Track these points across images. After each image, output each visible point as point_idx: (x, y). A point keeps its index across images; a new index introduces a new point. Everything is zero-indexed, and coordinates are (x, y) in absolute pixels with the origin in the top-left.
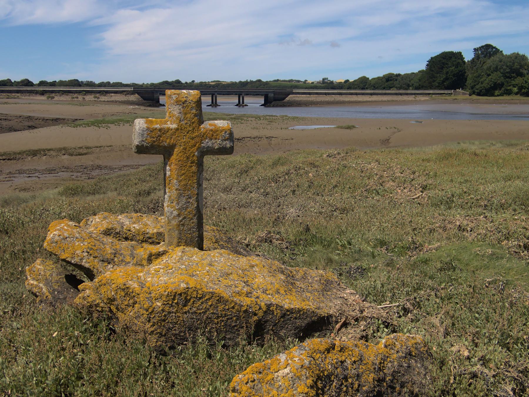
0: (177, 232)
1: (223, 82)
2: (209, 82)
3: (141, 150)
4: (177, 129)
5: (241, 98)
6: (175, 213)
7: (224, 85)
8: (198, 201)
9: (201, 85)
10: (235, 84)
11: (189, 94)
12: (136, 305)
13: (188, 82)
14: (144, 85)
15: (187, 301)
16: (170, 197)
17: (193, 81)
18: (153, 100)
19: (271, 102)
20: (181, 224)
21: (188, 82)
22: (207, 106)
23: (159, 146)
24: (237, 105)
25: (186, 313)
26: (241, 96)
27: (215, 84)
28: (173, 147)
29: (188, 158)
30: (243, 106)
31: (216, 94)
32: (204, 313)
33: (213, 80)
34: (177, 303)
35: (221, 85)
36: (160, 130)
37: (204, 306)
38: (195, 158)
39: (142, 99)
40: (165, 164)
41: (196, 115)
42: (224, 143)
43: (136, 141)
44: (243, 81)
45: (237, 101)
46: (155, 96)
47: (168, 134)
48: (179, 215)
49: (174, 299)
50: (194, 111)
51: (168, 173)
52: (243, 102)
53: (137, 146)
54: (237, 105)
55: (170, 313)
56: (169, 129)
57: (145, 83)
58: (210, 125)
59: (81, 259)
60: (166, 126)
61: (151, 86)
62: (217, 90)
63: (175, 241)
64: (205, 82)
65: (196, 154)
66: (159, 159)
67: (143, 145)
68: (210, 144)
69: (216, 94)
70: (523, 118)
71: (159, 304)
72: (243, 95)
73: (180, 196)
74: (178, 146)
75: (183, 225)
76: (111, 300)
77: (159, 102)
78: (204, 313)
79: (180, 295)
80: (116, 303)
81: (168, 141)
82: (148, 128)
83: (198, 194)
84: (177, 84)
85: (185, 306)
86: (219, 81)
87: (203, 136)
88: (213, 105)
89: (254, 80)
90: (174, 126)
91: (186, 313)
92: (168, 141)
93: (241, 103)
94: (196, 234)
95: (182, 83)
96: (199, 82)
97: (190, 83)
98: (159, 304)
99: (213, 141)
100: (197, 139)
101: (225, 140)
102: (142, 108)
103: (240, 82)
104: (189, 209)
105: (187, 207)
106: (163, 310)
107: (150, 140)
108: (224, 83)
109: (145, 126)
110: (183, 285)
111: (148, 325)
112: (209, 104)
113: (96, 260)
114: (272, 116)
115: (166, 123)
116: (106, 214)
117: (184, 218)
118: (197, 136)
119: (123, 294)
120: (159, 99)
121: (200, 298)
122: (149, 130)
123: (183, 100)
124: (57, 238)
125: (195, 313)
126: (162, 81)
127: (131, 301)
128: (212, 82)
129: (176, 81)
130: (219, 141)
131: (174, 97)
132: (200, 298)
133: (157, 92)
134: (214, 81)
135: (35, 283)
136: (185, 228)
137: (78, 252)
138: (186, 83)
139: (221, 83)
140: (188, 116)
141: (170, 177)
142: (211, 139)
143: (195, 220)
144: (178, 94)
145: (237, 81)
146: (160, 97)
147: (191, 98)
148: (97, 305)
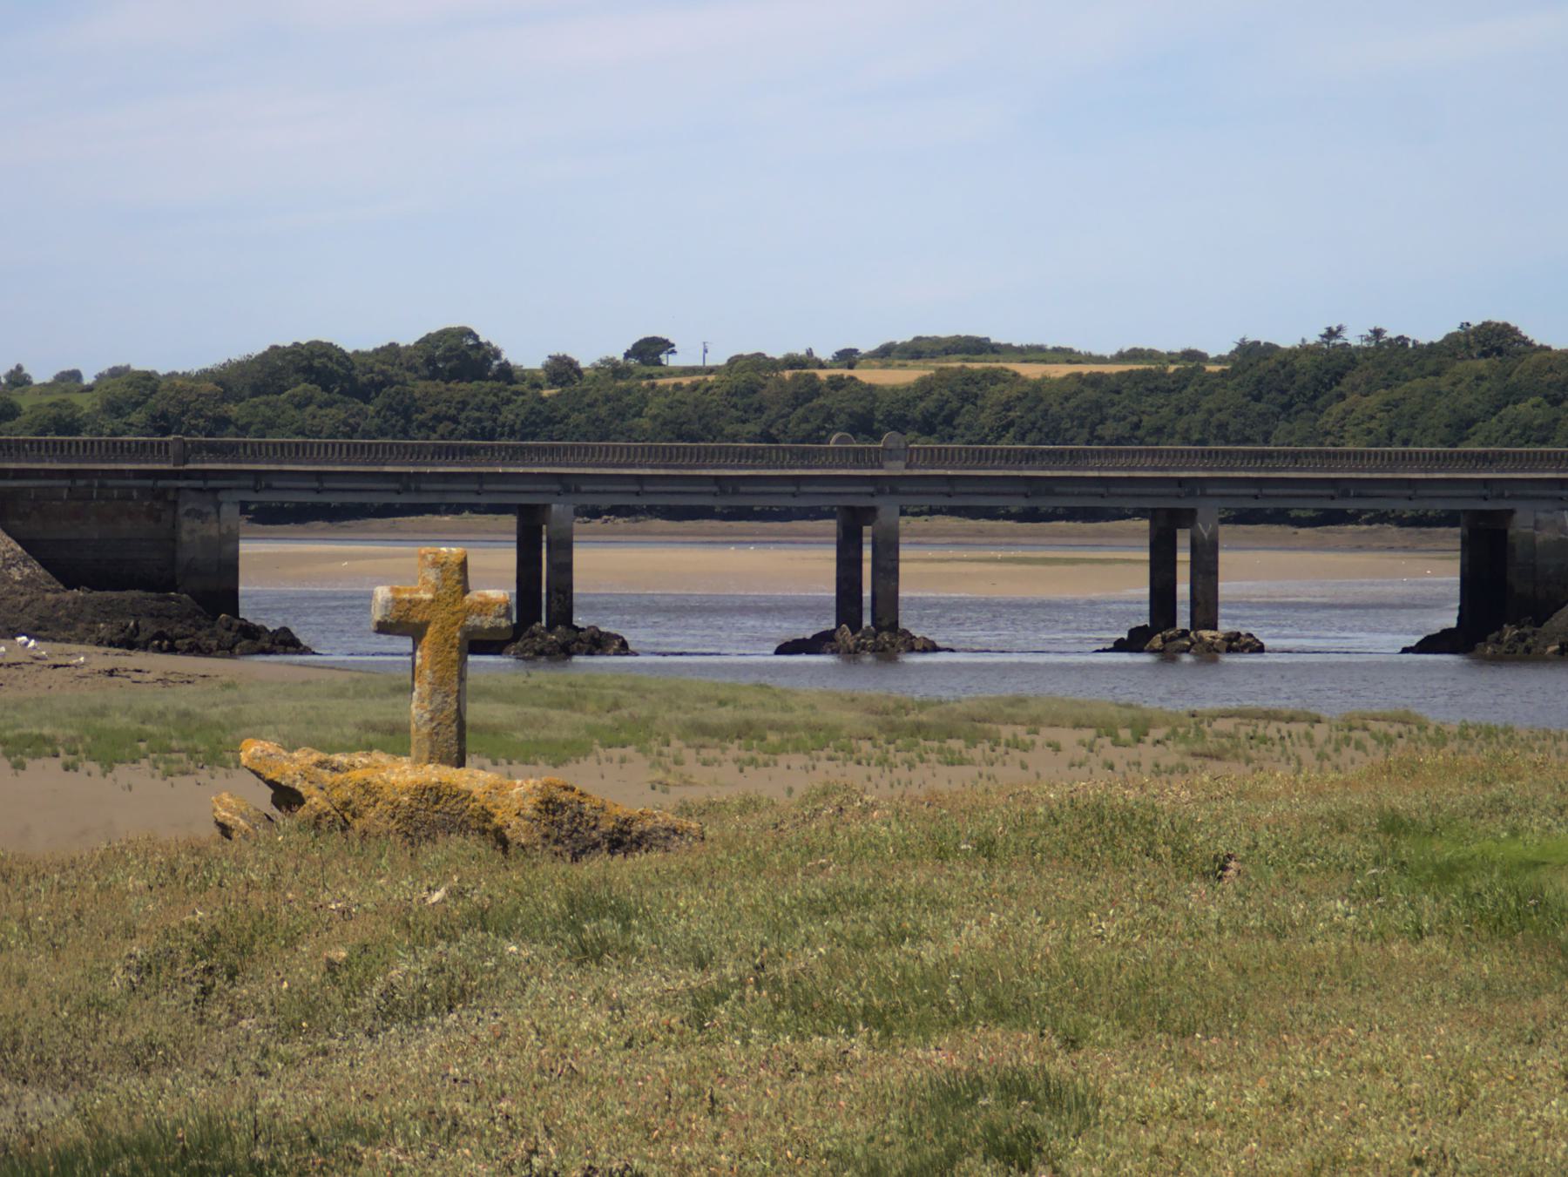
0: (428, 744)
1: (1034, 353)
2: (848, 357)
3: (383, 628)
4: (433, 601)
5: (1183, 556)
6: (427, 716)
7: (1037, 392)
8: (458, 700)
9: (752, 389)
10: (1182, 380)
11: (450, 552)
12: (379, 804)
13: (586, 359)
14: (25, 402)
15: (438, 800)
16: (420, 694)
17: (651, 350)
18: (161, 582)
19: (1540, 612)
20: (434, 733)
21: (584, 362)
22: (785, 649)
23: (407, 623)
24: (1134, 642)
25: (437, 812)
26: (1183, 539)
27: (925, 388)
28: (426, 624)
29: (446, 640)
30: (1209, 653)
31: (887, 508)
32: (459, 814)
33: (903, 336)
34: (427, 800)
35: (996, 393)
36: (410, 601)
37: (459, 806)
38: (456, 641)
39: (34, 569)
40: (415, 649)
41: (458, 582)
42: (498, 620)
43: (377, 615)
44: (1287, 338)
45: (1136, 589)
46: (193, 532)
47: (420, 607)
48: (432, 720)
49: (423, 794)
50: (456, 576)
51: (418, 661)
52: (1206, 607)
53: (379, 623)
54: (1134, 642)
55: (418, 809)
56: (421, 601)
57: (41, 373)
58: (480, 595)
59: (294, 781)
60: (416, 596)
61: (115, 408)
62: (896, 469)
63: (426, 756)
64: (792, 362)
65: (458, 634)
66: (406, 644)
67: (386, 622)
68: (477, 622)
69: (887, 508)
70: (1346, 601)
71: (406, 799)
72: (1204, 530)
73: (434, 692)
74: (432, 624)
75: (437, 734)
76: (346, 804)
77: (230, 599)
78: (459, 814)
79: (431, 789)
80: (352, 806)
81: (420, 616)
82: (394, 599)
83: (459, 691)
84: (437, 387)
85: (436, 803)
86: (977, 347)
87: (468, 611)
88: (846, 636)
89: (1428, 329)
90: (429, 596)
91: (437, 812)
92: (420, 616)
93: (1183, 622)
94: (455, 749)
95: (507, 373)
96: (718, 358)
97: (614, 370)
98: (406, 799)
99: (483, 618)
100: (460, 615)
101: (500, 617)
102: (86, 656)
103: (1250, 353)
104: (446, 713)
105: (442, 710)
106: (410, 806)
107: (395, 614)
108: (1031, 371)
109: (390, 595)
110: (434, 779)
111: (393, 823)
112: (807, 630)
113: (313, 787)
114: (1270, 716)
115: (417, 591)
116: (310, 749)
117: (439, 724)
118: (460, 611)
119: (362, 791)
120: (230, 568)
121: (455, 796)
122: (397, 602)
123: (442, 561)
124: (259, 754)
125: (448, 813)
126: (258, 347)
127: (372, 800)
128: (886, 354)
129: (427, 340)
130: (491, 618)
131: (430, 557)
132: (455, 796)
133: (211, 486)
134: (916, 350)
135: (228, 815)
136: (440, 739)
137: (290, 773)
138: (562, 370)
139: (994, 377)
140: (449, 582)
141: (421, 666)
142: (479, 615)
143: (454, 728)
144: (436, 554)
145: (1218, 343)
146: (247, 548)
147: (452, 559)
148: (327, 814)
